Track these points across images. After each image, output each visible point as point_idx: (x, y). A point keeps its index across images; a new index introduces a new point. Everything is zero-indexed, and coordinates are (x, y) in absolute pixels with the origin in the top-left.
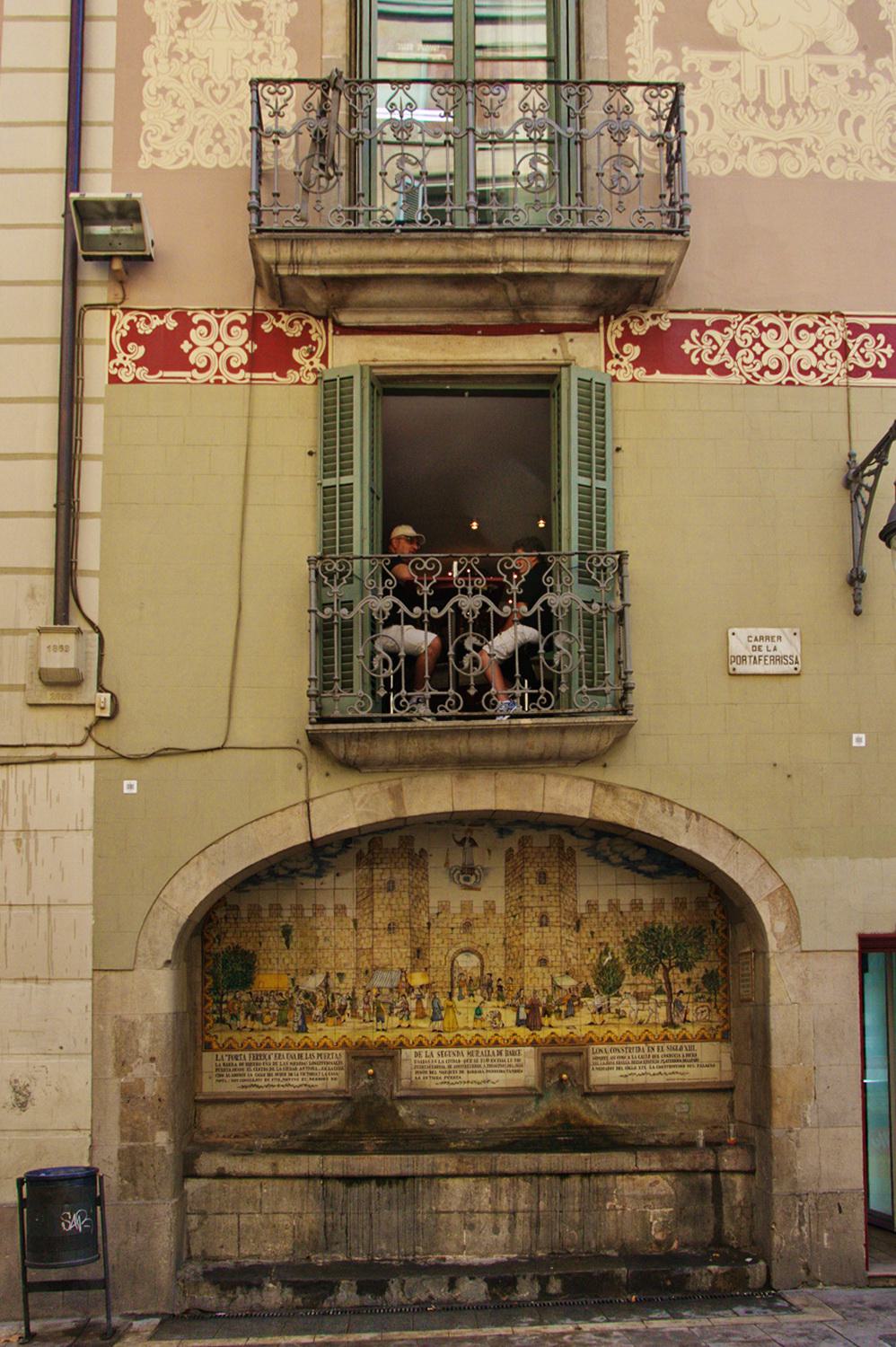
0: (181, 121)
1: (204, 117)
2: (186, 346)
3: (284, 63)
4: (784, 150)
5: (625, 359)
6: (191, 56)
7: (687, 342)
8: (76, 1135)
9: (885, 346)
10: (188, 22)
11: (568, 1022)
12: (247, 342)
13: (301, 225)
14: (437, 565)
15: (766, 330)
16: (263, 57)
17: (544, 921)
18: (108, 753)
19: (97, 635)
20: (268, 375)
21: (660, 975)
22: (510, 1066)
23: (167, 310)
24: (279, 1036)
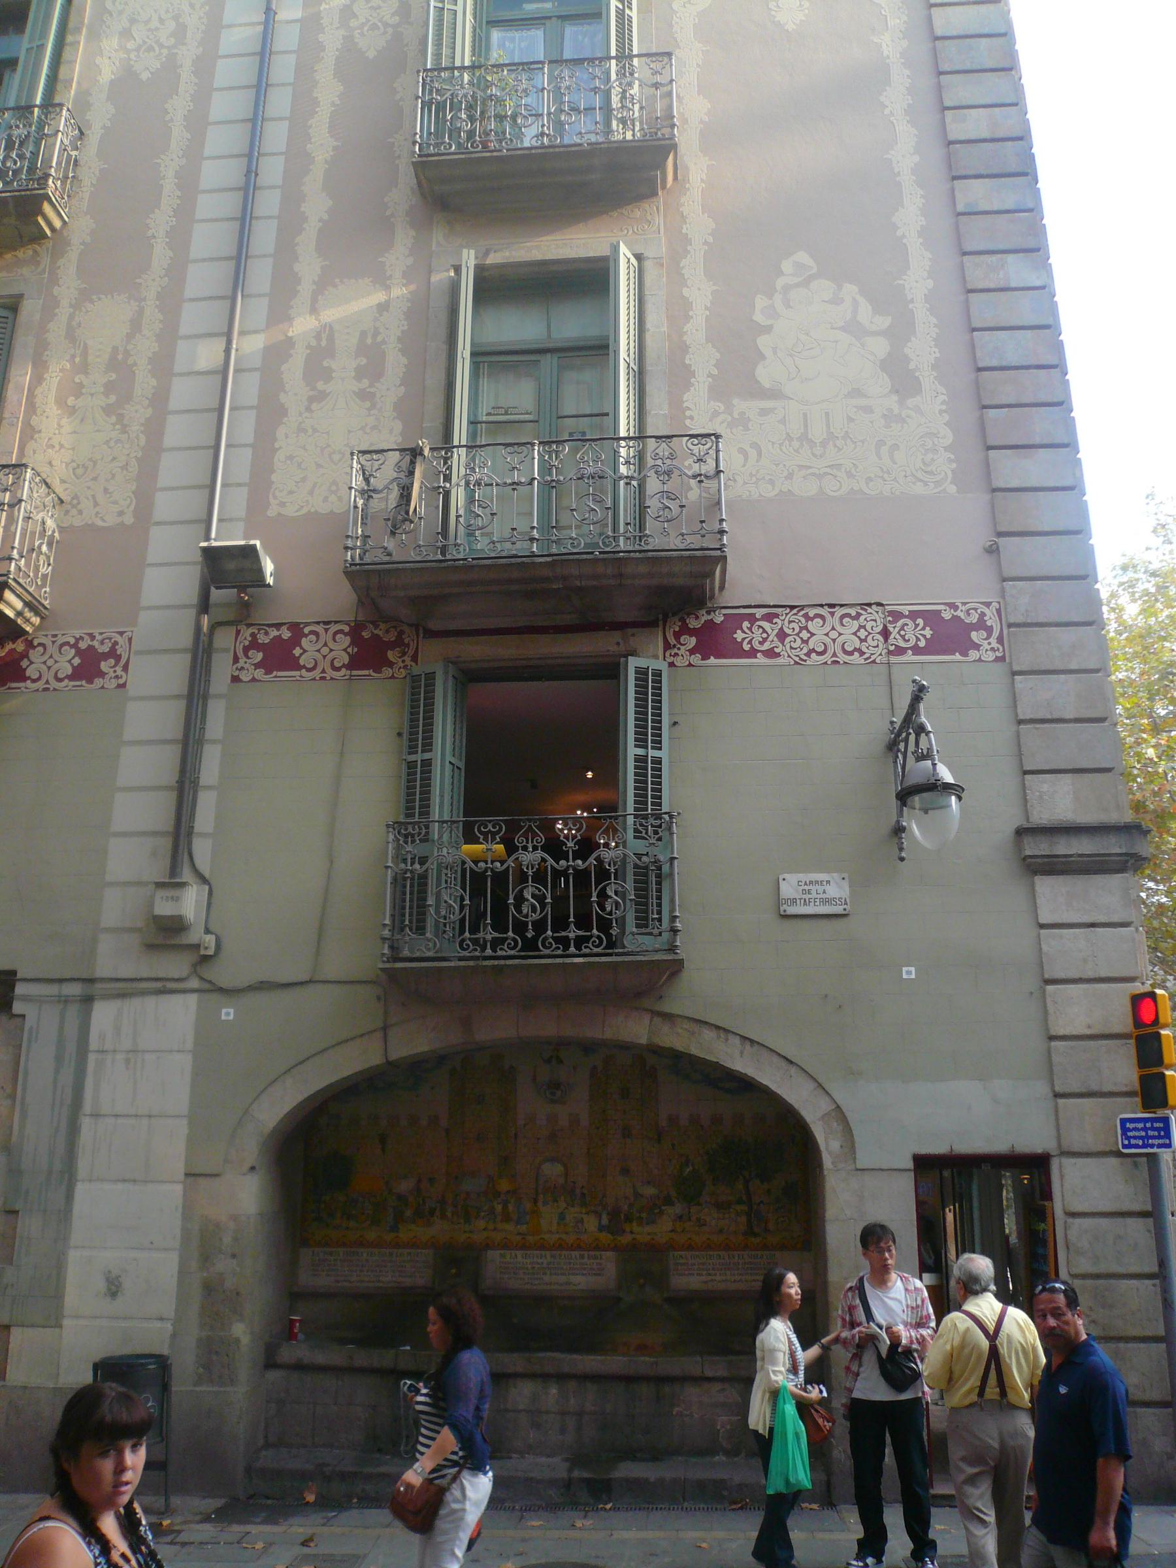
0: (304, 479)
2: (297, 652)
3: (391, 431)
4: (827, 474)
6: (315, 430)
7: (739, 631)
8: (159, 1324)
9: (923, 629)
11: (648, 1229)
13: (387, 559)
15: (812, 619)
16: (374, 428)
17: (626, 1133)
18: (207, 986)
19: (207, 887)
20: (366, 672)
21: (740, 1186)
22: (592, 1269)
24: (371, 1235)
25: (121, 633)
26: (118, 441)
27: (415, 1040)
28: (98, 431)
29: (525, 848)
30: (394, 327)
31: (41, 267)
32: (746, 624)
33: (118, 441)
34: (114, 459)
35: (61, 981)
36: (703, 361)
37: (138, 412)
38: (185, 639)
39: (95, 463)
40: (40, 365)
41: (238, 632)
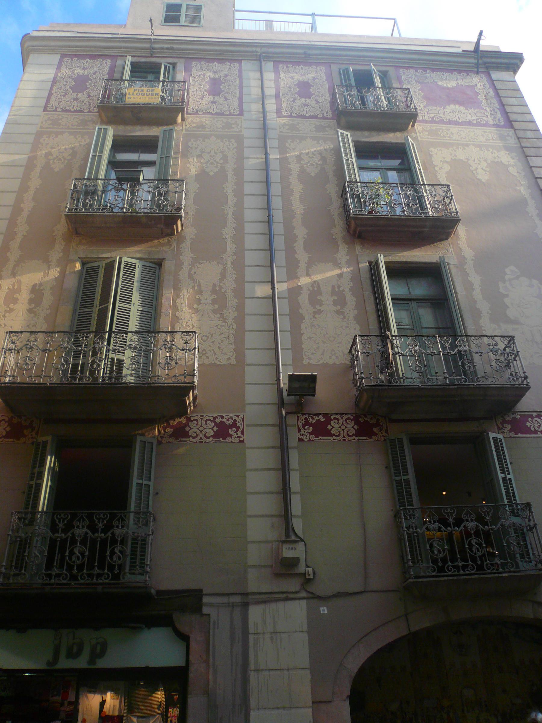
0: (318, 348)
1: (327, 346)
2: (329, 427)
3: (355, 329)
5: (506, 429)
10: (317, 316)
12: (354, 425)
14: (107, 516)
16: (347, 327)
18: (311, 596)
23: (321, 414)
25: (238, 416)
26: (222, 326)
27: (422, 621)
28: (212, 320)
29: (117, 527)
30: (347, 285)
31: (172, 248)
32: (530, 419)
33: (222, 326)
34: (221, 334)
35: (228, 595)
36: (484, 306)
37: (231, 314)
38: (272, 419)
39: (212, 335)
40: (177, 289)
41: (298, 417)
